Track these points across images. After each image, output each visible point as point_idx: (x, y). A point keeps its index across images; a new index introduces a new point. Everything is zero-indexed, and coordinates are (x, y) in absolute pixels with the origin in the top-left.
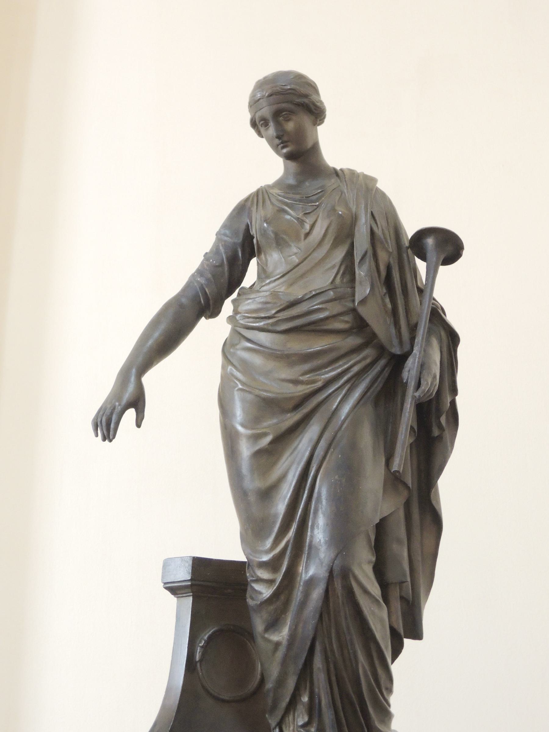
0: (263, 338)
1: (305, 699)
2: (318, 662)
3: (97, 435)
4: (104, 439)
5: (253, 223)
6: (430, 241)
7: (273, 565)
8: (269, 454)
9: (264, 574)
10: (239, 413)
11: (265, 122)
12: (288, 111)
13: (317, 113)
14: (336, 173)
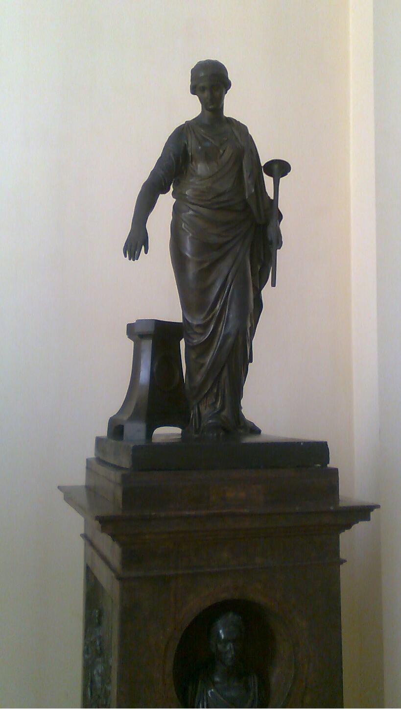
0: (201, 210)
1: (215, 391)
2: (225, 374)
3: (126, 256)
4: (130, 259)
5: (189, 143)
6: (276, 167)
7: (205, 326)
8: (205, 273)
9: (199, 330)
10: (188, 249)
11: (203, 89)
12: (211, 81)
13: (227, 85)
14: (230, 121)
